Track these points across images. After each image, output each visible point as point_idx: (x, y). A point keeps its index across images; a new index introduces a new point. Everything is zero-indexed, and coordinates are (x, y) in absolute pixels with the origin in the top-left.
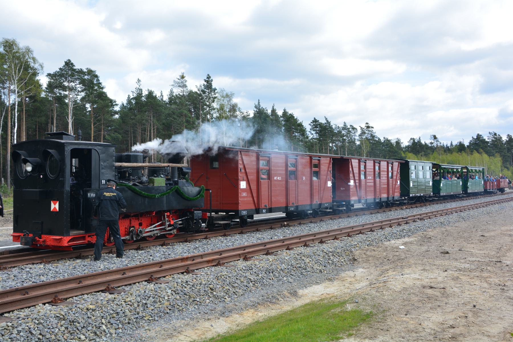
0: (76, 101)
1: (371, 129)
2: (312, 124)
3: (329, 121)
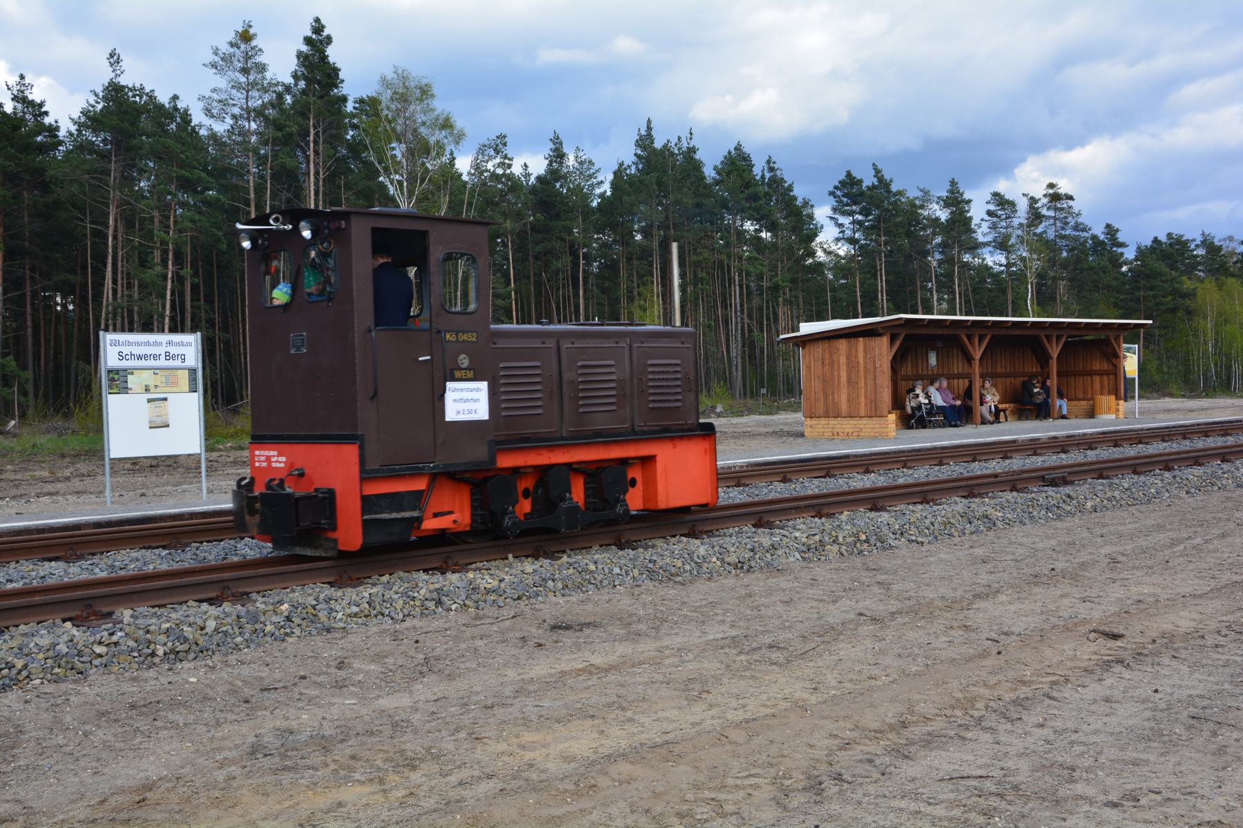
0: (1226, 263)
2: (838, 193)
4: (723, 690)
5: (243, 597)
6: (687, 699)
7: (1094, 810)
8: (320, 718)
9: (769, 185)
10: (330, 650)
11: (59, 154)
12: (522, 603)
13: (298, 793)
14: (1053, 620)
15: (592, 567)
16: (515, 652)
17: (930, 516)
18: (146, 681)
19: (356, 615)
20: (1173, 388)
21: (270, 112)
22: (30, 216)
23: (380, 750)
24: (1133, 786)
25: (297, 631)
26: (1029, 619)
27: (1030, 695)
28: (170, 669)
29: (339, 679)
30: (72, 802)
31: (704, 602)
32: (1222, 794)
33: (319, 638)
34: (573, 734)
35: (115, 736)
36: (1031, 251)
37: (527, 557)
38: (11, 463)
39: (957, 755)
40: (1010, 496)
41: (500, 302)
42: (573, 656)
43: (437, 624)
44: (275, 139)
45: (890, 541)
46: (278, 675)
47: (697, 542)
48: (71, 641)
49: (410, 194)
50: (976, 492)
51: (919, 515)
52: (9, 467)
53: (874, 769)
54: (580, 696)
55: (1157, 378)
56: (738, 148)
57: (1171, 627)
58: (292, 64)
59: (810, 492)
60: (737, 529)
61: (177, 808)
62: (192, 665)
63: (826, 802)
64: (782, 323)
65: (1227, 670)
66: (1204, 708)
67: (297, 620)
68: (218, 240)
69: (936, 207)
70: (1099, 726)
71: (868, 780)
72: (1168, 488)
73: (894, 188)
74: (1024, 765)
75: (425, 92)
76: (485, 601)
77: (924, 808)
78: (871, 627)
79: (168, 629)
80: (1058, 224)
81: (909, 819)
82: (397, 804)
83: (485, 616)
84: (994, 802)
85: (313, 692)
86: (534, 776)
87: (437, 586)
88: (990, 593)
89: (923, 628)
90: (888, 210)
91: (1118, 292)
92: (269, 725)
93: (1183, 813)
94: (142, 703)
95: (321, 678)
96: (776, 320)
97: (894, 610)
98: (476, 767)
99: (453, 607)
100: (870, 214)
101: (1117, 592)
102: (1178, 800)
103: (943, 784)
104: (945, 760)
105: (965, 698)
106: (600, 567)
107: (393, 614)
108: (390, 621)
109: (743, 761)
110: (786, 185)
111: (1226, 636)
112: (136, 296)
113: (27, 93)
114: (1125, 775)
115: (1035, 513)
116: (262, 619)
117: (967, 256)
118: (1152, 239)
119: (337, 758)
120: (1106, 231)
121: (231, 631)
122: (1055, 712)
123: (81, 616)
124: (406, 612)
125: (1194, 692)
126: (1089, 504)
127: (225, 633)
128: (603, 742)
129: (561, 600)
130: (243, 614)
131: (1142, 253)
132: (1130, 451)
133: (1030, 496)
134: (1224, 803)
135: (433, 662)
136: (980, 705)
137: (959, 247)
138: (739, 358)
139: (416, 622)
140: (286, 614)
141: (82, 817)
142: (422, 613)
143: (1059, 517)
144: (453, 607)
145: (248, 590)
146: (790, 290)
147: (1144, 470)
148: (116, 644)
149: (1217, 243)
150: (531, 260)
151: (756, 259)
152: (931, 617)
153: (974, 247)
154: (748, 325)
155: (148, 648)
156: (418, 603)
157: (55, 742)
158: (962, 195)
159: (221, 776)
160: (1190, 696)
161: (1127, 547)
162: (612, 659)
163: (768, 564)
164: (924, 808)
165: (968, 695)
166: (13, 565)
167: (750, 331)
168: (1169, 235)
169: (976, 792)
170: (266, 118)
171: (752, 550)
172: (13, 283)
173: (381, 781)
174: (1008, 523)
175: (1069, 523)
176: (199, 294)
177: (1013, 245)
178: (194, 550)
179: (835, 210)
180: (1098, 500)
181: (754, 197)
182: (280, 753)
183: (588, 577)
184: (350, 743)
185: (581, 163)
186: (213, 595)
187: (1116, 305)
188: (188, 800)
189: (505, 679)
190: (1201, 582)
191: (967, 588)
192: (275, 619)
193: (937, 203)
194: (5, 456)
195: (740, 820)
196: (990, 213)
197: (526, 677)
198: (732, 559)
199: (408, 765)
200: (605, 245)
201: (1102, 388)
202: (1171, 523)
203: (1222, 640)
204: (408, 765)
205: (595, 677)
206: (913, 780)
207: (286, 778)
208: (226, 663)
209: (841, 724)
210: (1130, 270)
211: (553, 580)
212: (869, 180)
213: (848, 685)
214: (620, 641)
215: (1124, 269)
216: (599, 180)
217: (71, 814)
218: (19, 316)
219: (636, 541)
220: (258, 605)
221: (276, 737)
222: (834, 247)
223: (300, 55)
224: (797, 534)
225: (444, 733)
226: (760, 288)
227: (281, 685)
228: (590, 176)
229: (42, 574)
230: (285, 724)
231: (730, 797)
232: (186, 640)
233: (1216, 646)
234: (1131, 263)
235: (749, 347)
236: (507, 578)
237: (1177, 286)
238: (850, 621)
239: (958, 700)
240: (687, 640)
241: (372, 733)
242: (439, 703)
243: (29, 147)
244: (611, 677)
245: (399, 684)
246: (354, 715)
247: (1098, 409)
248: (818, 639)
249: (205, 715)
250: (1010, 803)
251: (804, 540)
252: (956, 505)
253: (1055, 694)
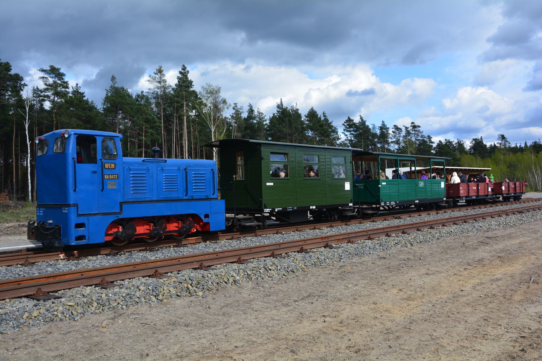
1: (417, 129)
2: (346, 124)
58: (176, 81)
80: (416, 136)
118: (439, 141)
179: (344, 130)
185: (259, 113)
216: (265, 119)
223: (178, 78)
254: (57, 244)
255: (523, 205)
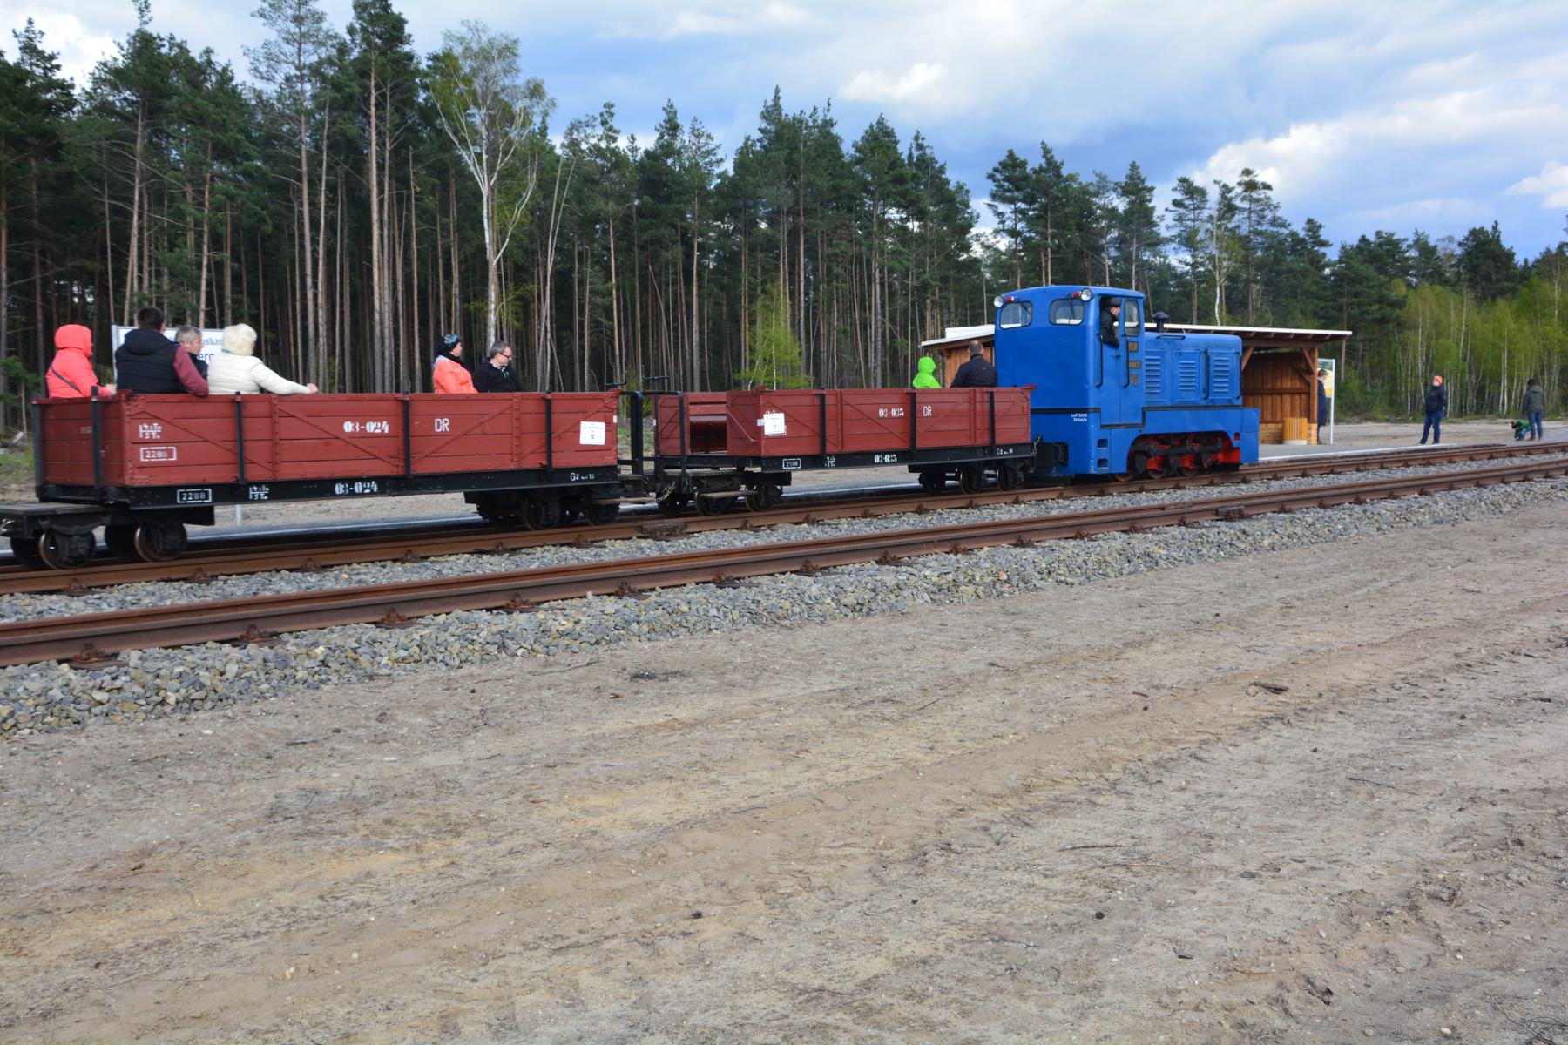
1: (1260, 194)
2: (998, 176)
3: (1056, 159)
4: (825, 749)
5: (271, 638)
6: (782, 759)
7: (1228, 881)
8: (352, 777)
9: (918, 166)
10: (370, 699)
11: (75, 114)
12: (600, 649)
13: (321, 862)
14: (1211, 672)
15: (685, 608)
16: (587, 704)
17: (1082, 554)
18: (154, 733)
19: (404, 660)
20: (1377, 412)
21: (330, 71)
22: (39, 188)
23: (420, 814)
24: (1275, 855)
25: (334, 678)
26: (1184, 671)
27: (1175, 756)
28: (183, 720)
29: (379, 733)
30: (58, 867)
31: (813, 649)
32: (1370, 862)
33: (359, 686)
34: (647, 798)
35: (113, 794)
36: (1220, 249)
37: (609, 595)
38: (17, 481)
39: (1085, 823)
40: (1176, 531)
41: (599, 300)
42: (653, 710)
43: (498, 671)
44: (333, 101)
45: (1035, 582)
46: (307, 727)
47: (809, 580)
48: (67, 685)
49: (491, 170)
50: (1138, 526)
51: (1070, 552)
52: (14, 486)
53: (988, 838)
54: (658, 754)
55: (1358, 399)
56: (881, 122)
57: (1341, 679)
59: (947, 524)
60: (857, 566)
61: (178, 876)
62: (208, 715)
63: (929, 875)
64: (929, 329)
65: (1396, 727)
66: (1364, 768)
67: (334, 666)
68: (262, 221)
69: (1113, 195)
70: (1247, 789)
71: (980, 850)
72: (1357, 523)
73: (1065, 172)
74: (1157, 833)
75: (508, 50)
76: (557, 646)
77: (1039, 881)
78: (1004, 679)
79: (181, 674)
80: (1254, 217)
81: (1020, 893)
82: (435, 875)
83: (556, 663)
84: (1119, 873)
85: (347, 748)
86: (597, 845)
87: (501, 628)
88: (1142, 641)
89: (1063, 680)
90: (1057, 198)
91: (1320, 299)
92: (293, 784)
93: (1323, 882)
94: (147, 758)
95: (359, 732)
96: (923, 327)
97: (1031, 660)
98: (531, 833)
99: (519, 652)
100: (1036, 202)
101: (1287, 641)
102: (1322, 869)
103: (1064, 855)
104: (1067, 829)
105: (1101, 759)
106: (694, 608)
107: (447, 660)
108: (444, 668)
109: (839, 828)
110: (937, 166)
111: (1400, 689)
112: (166, 287)
113: (36, 42)
114: (1268, 843)
115: (1204, 551)
116: (293, 663)
117: (1148, 253)
118: (1359, 237)
119: (368, 822)
120: (1307, 227)
121: (255, 677)
122: (1201, 774)
123: (80, 657)
124: (463, 657)
125: (1356, 751)
126: (1266, 542)
127: (249, 679)
128: (680, 807)
129: (646, 646)
130: (270, 657)
131: (1346, 253)
132: (1318, 482)
133: (1199, 531)
134: (1369, 871)
135: (489, 714)
136: (1117, 767)
137: (1138, 242)
138: (879, 370)
139: (475, 669)
140: (321, 658)
141: (67, 885)
142: (482, 659)
143: (1232, 556)
144: (519, 652)
145: (278, 630)
146: (941, 290)
147: (1332, 503)
148: (119, 689)
149: (1432, 243)
150: (637, 251)
151: (901, 253)
152: (1073, 668)
153: (1155, 243)
154: (891, 331)
155: (157, 694)
156: (477, 647)
157: (42, 801)
158: (1143, 181)
159: (232, 841)
160: (1352, 755)
161: (1305, 591)
162: (699, 713)
163: (892, 607)
164: (1039, 881)
165: (1105, 756)
166: (7, 598)
167: (893, 337)
168: (1378, 234)
169: (1100, 863)
170: (324, 78)
171: (873, 590)
172: (19, 267)
173: (419, 849)
174: (1173, 562)
175: (1241, 562)
176: (241, 285)
177: (1201, 241)
178: (221, 583)
180: (1277, 536)
181: (900, 180)
182: (303, 816)
183: (679, 619)
184: (386, 805)
186: (236, 635)
187: (1315, 314)
188: (192, 867)
189: (573, 734)
190: (1381, 629)
191: (1118, 636)
192: (308, 663)
193: (1115, 190)
194: (9, 473)
195: (829, 895)
196: (1177, 203)
197: (597, 732)
198: (850, 600)
199: (451, 831)
200: (724, 234)
201: (1293, 408)
202: (1356, 563)
203: (1394, 694)
204: (451, 831)
205: (678, 733)
206: (1030, 850)
207: (308, 844)
208: (248, 714)
209: (956, 787)
210: (1333, 274)
211: (638, 623)
212: (1035, 161)
213: (970, 745)
214: (711, 692)
215: (1327, 271)
216: (719, 157)
217: (55, 881)
218: (527, 340)
219: (738, 579)
220: (289, 647)
221: (300, 797)
222: (992, 240)
224: (927, 572)
225: (496, 795)
226: (904, 287)
227: (310, 739)
228: (709, 153)
229: (40, 609)
230: (311, 784)
231: (820, 868)
232: (202, 686)
233: (1388, 700)
234: (1334, 264)
235: (891, 358)
236: (584, 619)
237: (1386, 292)
238: (980, 672)
239: (1093, 761)
240: (787, 691)
241: (412, 795)
242: (494, 762)
243: (33, 104)
244: (696, 734)
245: (448, 739)
246: (393, 774)
247: (1287, 434)
248: (941, 692)
249: (220, 772)
250: (1136, 875)
251: (935, 579)
252: (1115, 541)
253: (1202, 754)
254: (1054, 474)
255: (1256, 488)
